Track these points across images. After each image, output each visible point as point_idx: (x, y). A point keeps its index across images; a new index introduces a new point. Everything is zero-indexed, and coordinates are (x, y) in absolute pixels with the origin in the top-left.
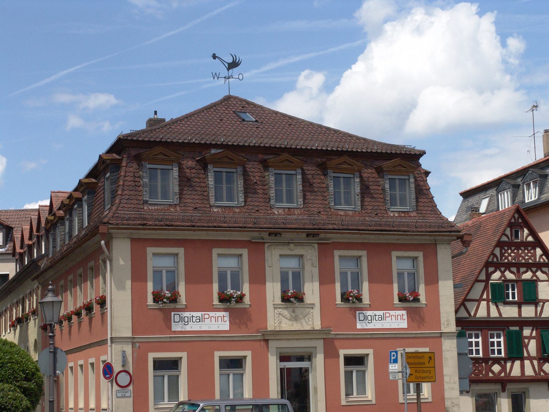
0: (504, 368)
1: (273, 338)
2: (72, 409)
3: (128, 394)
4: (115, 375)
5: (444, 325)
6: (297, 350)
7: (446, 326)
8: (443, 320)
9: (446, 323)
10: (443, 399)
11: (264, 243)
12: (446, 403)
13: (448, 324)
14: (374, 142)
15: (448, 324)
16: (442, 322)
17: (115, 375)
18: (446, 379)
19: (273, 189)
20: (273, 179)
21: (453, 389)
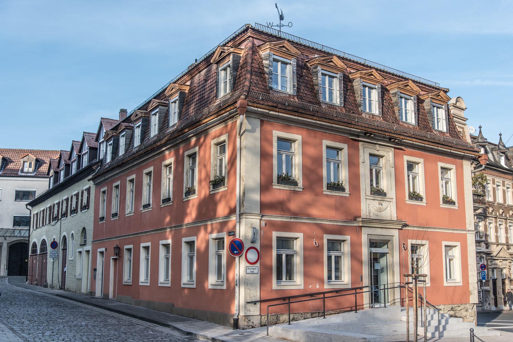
11: (359, 141)
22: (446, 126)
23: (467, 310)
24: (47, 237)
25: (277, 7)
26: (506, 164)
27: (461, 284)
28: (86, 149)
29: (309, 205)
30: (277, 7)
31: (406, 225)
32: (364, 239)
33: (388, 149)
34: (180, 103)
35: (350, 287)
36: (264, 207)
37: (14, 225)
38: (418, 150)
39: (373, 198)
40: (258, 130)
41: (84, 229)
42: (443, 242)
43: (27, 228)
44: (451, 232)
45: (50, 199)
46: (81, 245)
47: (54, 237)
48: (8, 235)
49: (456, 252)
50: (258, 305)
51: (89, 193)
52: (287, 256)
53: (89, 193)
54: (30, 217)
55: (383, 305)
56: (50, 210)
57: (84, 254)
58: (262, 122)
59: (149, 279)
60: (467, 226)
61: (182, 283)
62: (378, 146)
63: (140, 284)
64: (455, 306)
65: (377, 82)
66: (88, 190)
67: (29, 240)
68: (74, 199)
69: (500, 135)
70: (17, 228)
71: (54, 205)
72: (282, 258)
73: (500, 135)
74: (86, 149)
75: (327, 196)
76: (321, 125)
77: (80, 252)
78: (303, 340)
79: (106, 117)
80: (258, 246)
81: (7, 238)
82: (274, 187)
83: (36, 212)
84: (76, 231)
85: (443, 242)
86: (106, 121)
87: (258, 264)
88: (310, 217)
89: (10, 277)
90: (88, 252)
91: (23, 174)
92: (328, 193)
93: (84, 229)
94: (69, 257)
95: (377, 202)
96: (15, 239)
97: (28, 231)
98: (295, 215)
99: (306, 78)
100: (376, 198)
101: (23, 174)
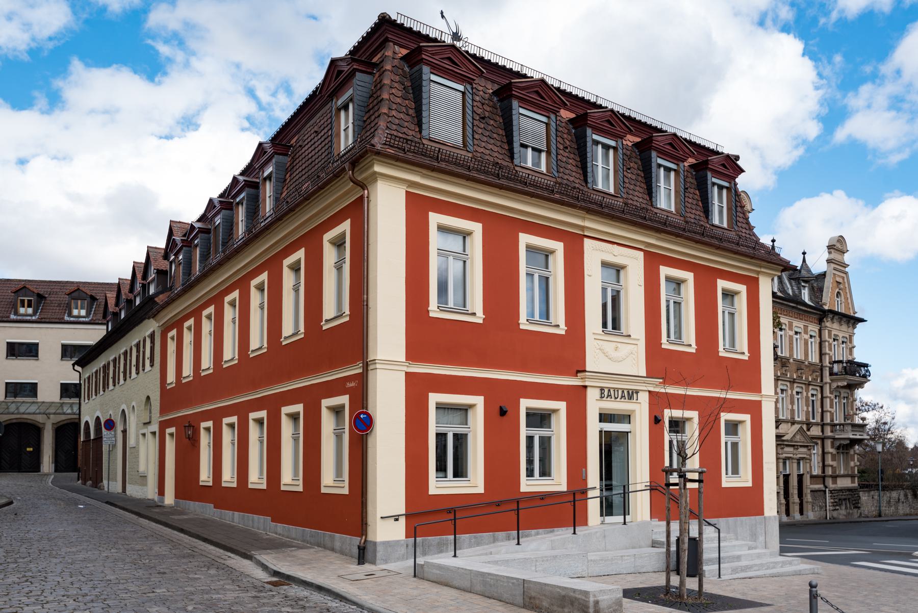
24: (102, 412)
25: (443, 17)
26: (811, 299)
28: (152, 275)
30: (443, 17)
34: (277, 180)
37: (61, 397)
41: (148, 398)
42: (722, 414)
43: (76, 400)
45: (103, 355)
46: (145, 424)
47: (111, 412)
48: (52, 410)
49: (745, 435)
51: (153, 342)
52: (455, 435)
53: (153, 342)
54: (80, 384)
56: (104, 372)
57: (149, 436)
59: (236, 476)
61: (282, 483)
63: (323, 490)
66: (152, 336)
67: (80, 418)
68: (134, 350)
69: (804, 253)
70: (67, 400)
71: (109, 363)
72: (446, 440)
73: (804, 253)
74: (152, 275)
77: (144, 435)
79: (178, 220)
81: (52, 416)
83: (87, 376)
84: (138, 402)
85: (722, 414)
86: (179, 225)
89: (57, 474)
90: (154, 433)
91: (72, 319)
93: (148, 398)
94: (131, 442)
96: (63, 417)
97: (570, 507)
99: (492, 122)
101: (72, 319)
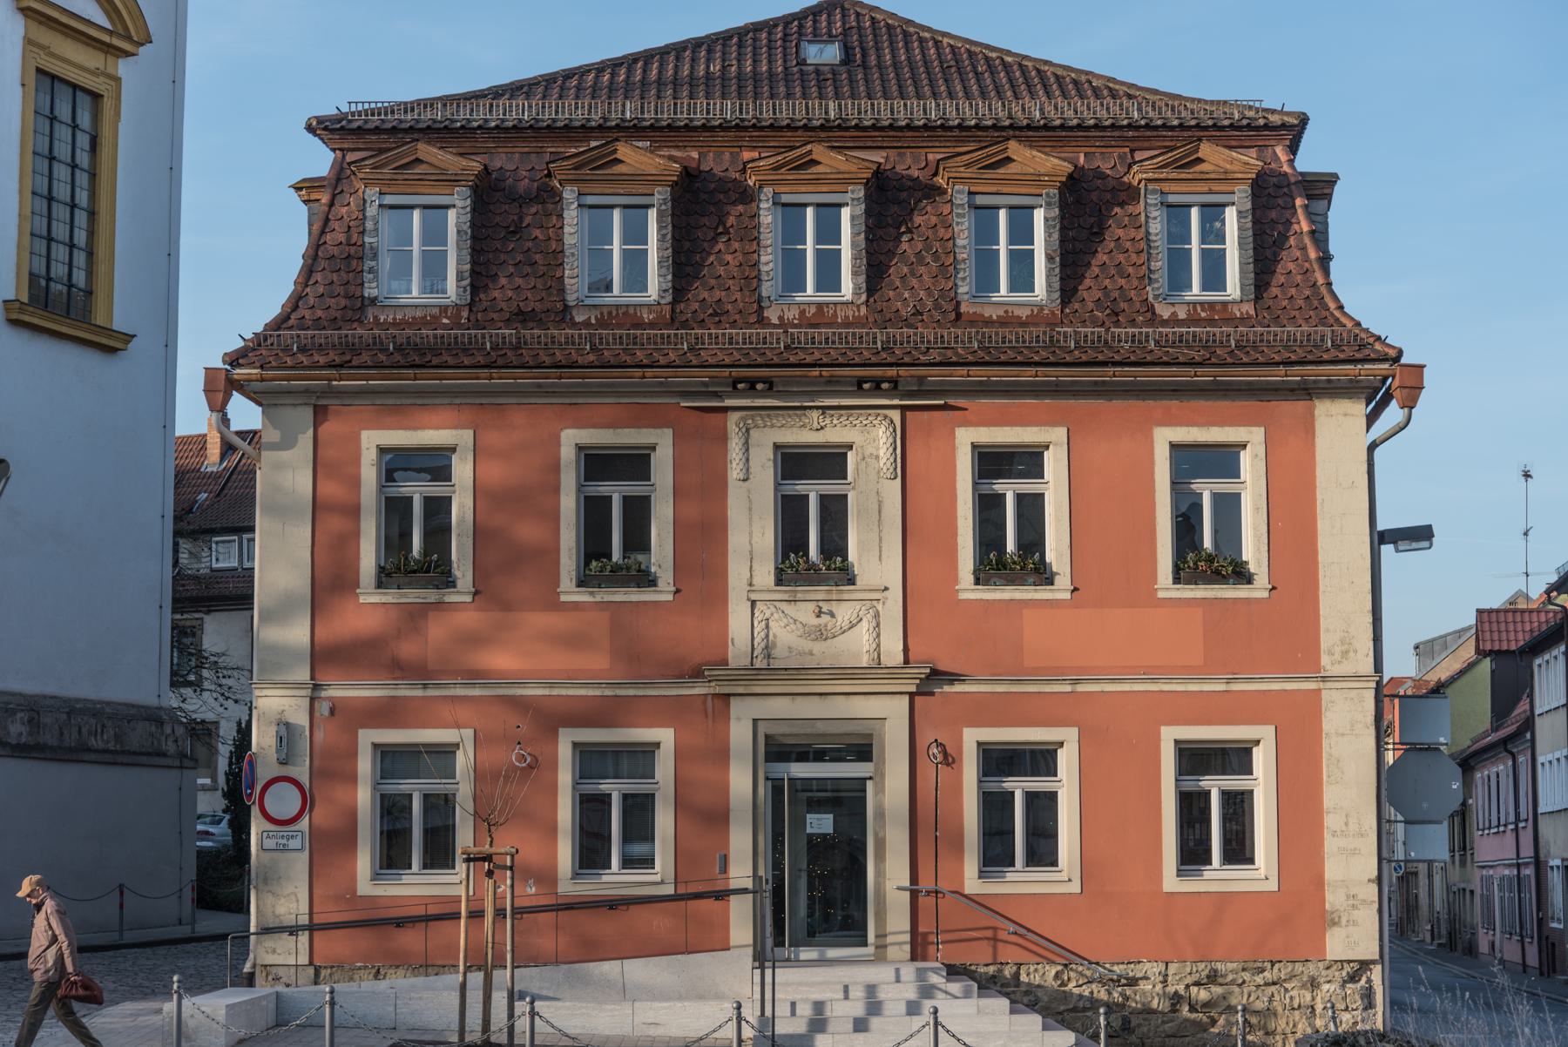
0: (1527, 864)
1: (741, 690)
2: (897, 970)
3: (295, 844)
4: (258, 788)
5: (1331, 653)
6: (821, 727)
7: (1337, 656)
8: (1328, 639)
9: (1337, 650)
10: (1319, 882)
11: (726, 409)
12: (1329, 897)
13: (1345, 653)
14: (1132, 92)
15: (1345, 653)
16: (1324, 645)
17: (258, 788)
18: (1331, 822)
19: (769, 250)
20: (770, 219)
21: (1354, 852)
22: (1242, 271)
23: (1313, 984)
27: (1272, 886)
29: (474, 640)
31: (937, 676)
32: (740, 733)
33: (862, 418)
35: (669, 890)
36: (323, 657)
38: (985, 397)
39: (786, 597)
40: (306, 440)
44: (1068, 688)
50: (304, 938)
55: (870, 950)
58: (320, 414)
60: (1325, 660)
62: (815, 414)
64: (1230, 966)
65: (455, 181)
75: (576, 606)
76: (1250, 383)
78: (222, 1041)
80: (302, 772)
82: (362, 600)
87: (304, 824)
88: (475, 676)
92: (583, 597)
95: (811, 606)
98: (419, 672)
100: (799, 596)
